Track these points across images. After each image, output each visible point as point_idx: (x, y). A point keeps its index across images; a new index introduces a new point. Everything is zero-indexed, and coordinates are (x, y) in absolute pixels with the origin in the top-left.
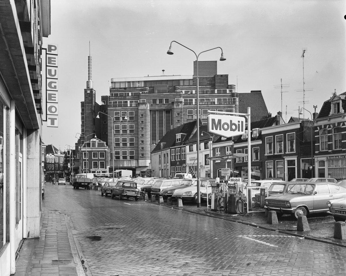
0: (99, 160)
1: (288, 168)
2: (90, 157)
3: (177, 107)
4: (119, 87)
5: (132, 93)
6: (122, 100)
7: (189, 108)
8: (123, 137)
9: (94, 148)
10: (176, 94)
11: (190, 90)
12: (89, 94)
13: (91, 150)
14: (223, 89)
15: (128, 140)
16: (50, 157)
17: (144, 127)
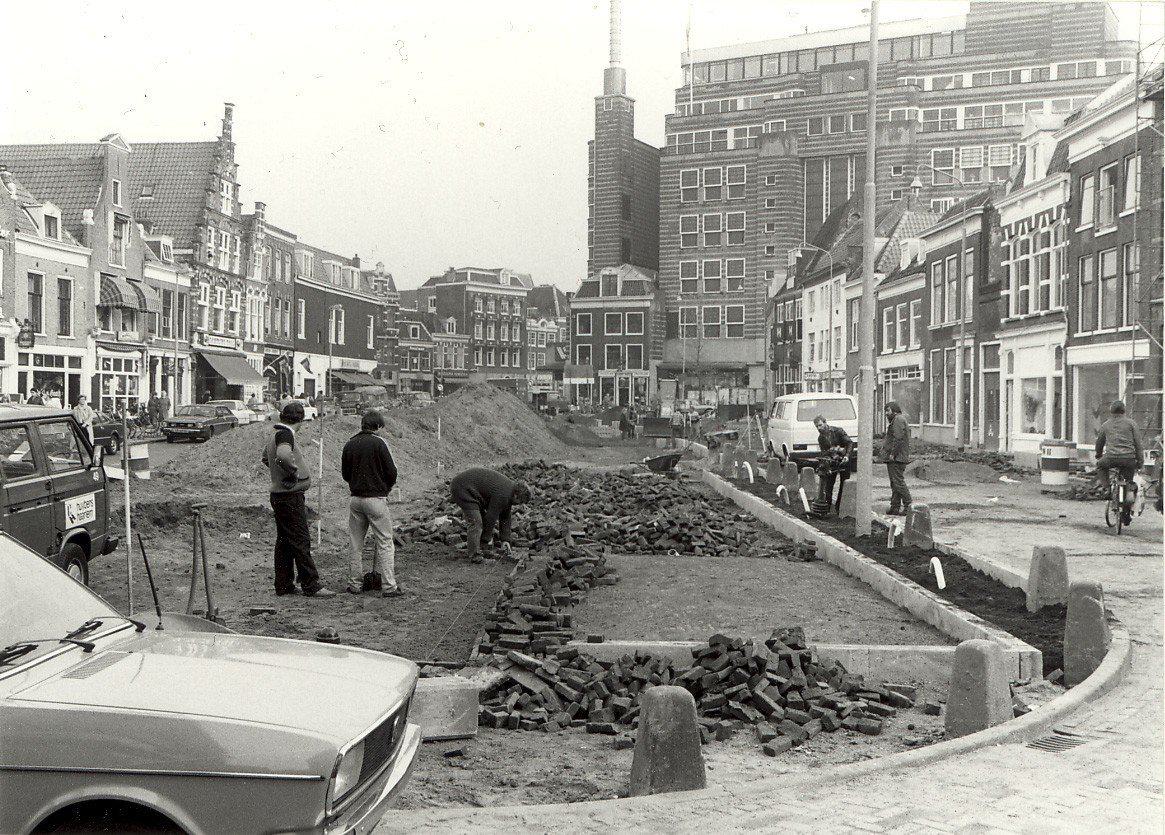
0: (624, 339)
1: (121, 360)
2: (599, 330)
4: (848, 59)
5: (746, 101)
6: (707, 127)
7: (940, 142)
8: (707, 257)
9: (612, 297)
10: (893, 94)
11: (953, 75)
12: (614, 116)
13: (600, 305)
14: (1082, 61)
15: (724, 269)
16: (541, 329)
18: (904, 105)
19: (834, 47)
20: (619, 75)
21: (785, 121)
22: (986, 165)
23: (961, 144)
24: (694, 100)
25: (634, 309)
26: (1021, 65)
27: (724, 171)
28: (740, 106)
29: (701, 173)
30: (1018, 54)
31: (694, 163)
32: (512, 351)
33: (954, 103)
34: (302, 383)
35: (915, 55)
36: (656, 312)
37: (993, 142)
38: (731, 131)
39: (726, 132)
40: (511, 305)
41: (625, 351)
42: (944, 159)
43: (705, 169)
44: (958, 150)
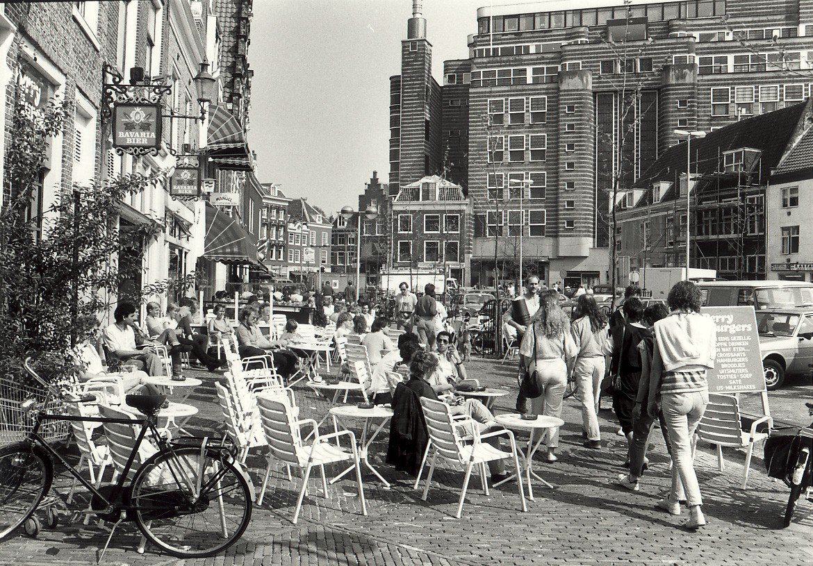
0: (442, 236)
3: (680, 82)
6: (510, 65)
7: (715, 82)
17: (577, 142)
18: (685, 52)
19: (565, 11)
20: (421, 23)
21: (580, 62)
22: (757, 101)
23: (735, 84)
24: (493, 44)
25: (451, 211)
26: (773, 25)
27: (528, 100)
28: (532, 50)
29: (506, 101)
31: (500, 94)
32: (278, 227)
33: (798, 48)
34: (466, 260)
35: (683, 16)
36: (470, 214)
37: (763, 83)
38: (529, 70)
39: (525, 70)
40: (278, 212)
41: (442, 246)
42: (721, 95)
43: (510, 98)
44: (733, 88)
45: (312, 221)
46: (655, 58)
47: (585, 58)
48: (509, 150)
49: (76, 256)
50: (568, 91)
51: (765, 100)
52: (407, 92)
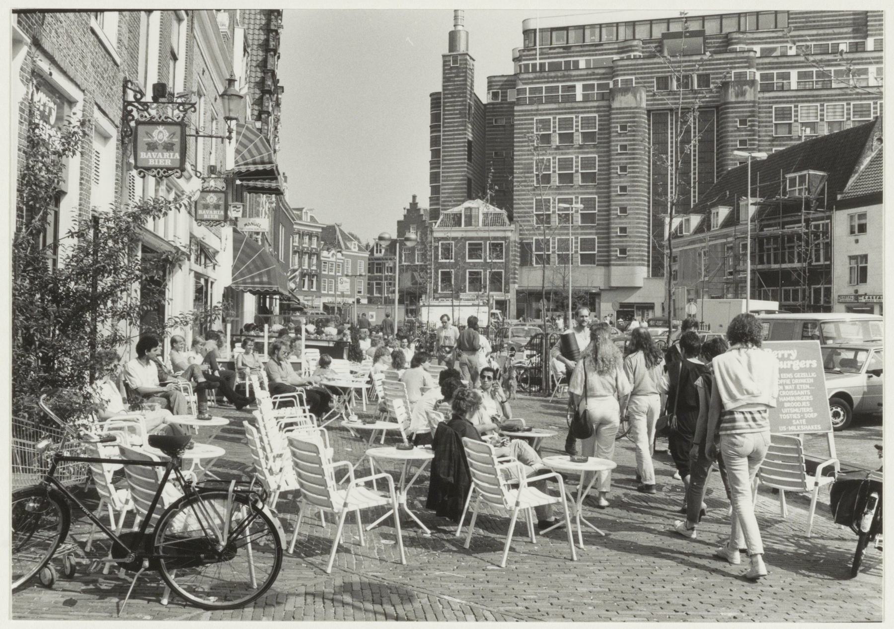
0: (485, 265)
2: (460, 255)
3: (740, 99)
5: (588, 62)
11: (779, 45)
16: (331, 259)
17: (630, 163)
18: (745, 67)
21: (633, 77)
22: (822, 120)
23: (799, 102)
25: (495, 238)
26: (839, 39)
27: (577, 119)
28: (582, 65)
30: (836, 31)
33: (866, 63)
35: (742, 29)
37: (829, 101)
38: (579, 86)
39: (574, 87)
40: (310, 239)
41: (486, 275)
42: (784, 114)
44: (796, 107)
45: (347, 248)
46: (713, 74)
47: (638, 74)
48: (558, 172)
49: (94, 286)
50: (620, 109)
51: (831, 119)
52: (449, 110)
